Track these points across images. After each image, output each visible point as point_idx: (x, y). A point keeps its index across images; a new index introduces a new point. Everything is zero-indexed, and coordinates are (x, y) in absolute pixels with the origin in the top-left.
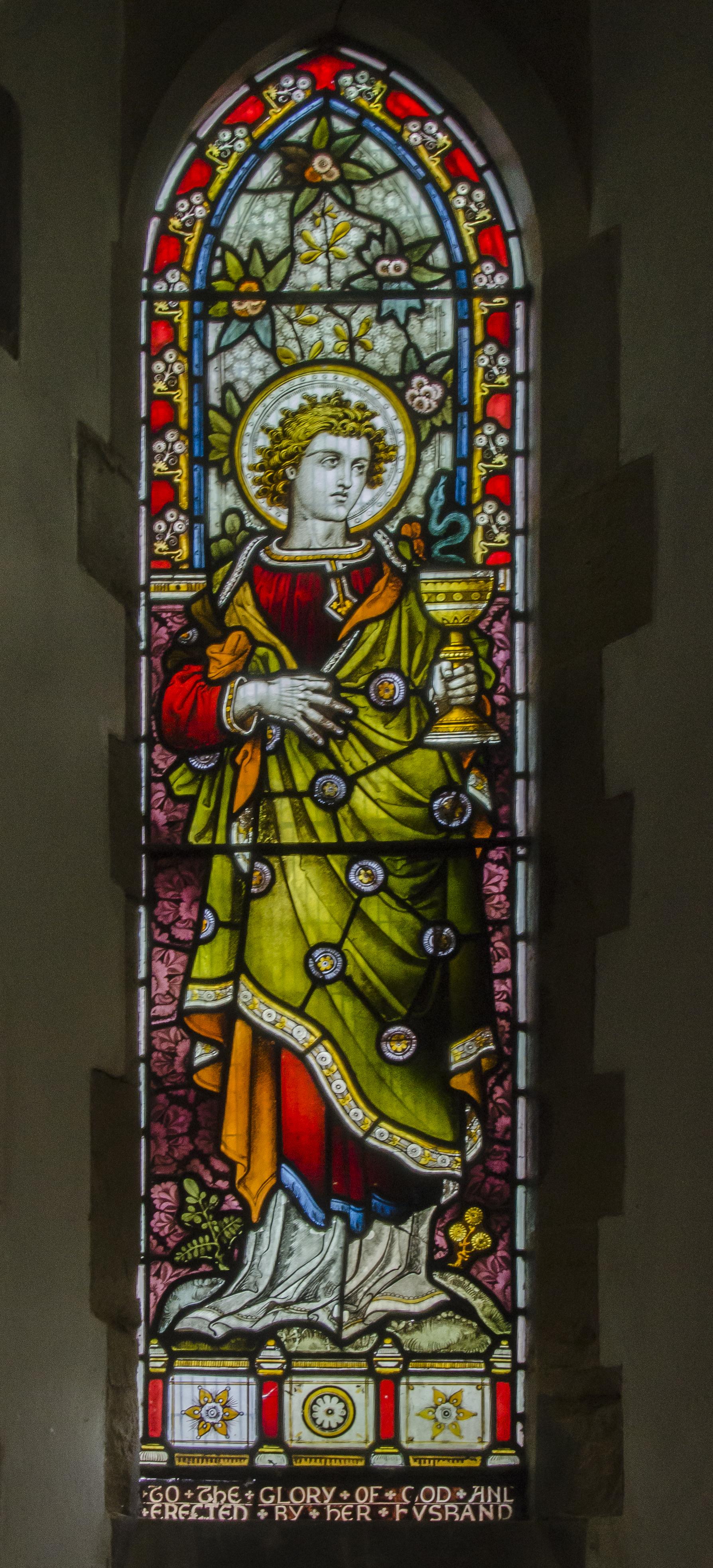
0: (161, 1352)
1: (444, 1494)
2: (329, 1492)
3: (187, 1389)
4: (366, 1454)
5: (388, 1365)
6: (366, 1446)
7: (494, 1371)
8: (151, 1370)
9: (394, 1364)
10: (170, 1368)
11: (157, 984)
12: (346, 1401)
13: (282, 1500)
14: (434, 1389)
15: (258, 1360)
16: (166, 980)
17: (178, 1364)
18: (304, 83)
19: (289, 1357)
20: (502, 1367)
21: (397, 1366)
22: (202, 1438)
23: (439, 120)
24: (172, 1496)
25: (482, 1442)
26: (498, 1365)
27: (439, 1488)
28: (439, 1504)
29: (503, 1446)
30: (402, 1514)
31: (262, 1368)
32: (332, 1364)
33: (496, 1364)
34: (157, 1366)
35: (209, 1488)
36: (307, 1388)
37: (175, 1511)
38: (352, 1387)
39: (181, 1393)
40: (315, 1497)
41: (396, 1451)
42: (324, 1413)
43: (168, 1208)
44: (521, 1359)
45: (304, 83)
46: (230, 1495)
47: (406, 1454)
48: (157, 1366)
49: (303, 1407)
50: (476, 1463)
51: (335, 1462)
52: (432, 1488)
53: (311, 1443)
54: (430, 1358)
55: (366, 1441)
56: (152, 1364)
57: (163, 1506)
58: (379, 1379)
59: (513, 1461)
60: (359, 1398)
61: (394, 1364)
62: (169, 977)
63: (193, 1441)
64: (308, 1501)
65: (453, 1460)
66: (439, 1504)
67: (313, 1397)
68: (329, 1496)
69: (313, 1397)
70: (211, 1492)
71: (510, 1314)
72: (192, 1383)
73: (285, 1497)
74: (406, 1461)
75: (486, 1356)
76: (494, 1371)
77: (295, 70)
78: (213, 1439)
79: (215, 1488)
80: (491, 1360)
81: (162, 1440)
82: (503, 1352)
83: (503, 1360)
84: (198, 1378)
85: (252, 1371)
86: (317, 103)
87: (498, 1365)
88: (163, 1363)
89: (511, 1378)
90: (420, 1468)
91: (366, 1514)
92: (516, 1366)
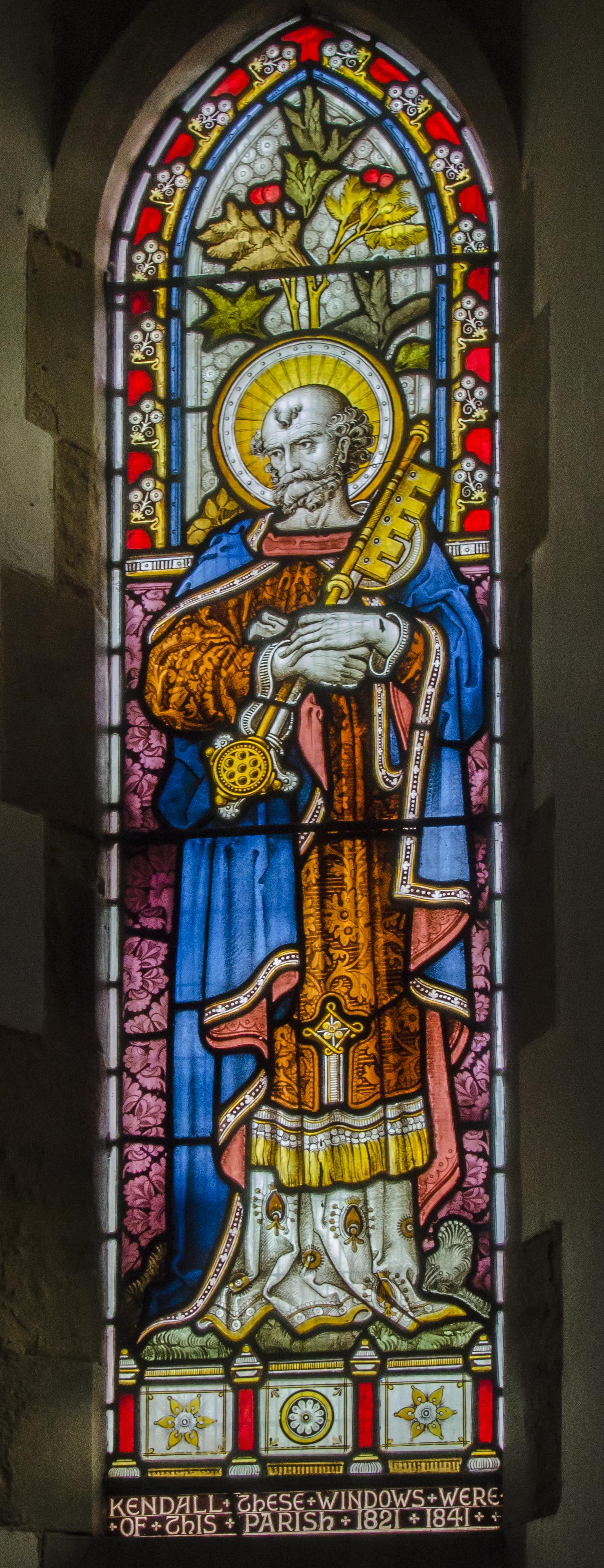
0: (132, 1363)
6: (222, 1456)
8: (121, 1382)
9: (370, 1367)
10: (382, 1370)
11: (129, 979)
12: (325, 1407)
15: (233, 1369)
16: (140, 974)
17: (149, 1374)
18: (290, 52)
19: (384, 1356)
20: (482, 1364)
23: (186, 118)
24: (371, 1502)
25: (223, 1451)
26: (240, 1374)
27: (162, 1499)
28: (212, 1514)
29: (366, 1451)
30: (140, 1529)
31: (238, 1377)
33: (476, 1361)
34: (127, 1378)
35: (247, 1497)
36: (284, 1393)
38: (327, 1389)
40: (481, 1499)
43: (472, 1193)
45: (290, 52)
46: (269, 1503)
47: (263, 1461)
48: (127, 1378)
49: (281, 1411)
51: (307, 1470)
55: (223, 1450)
56: (122, 1376)
60: (337, 1402)
61: (370, 1367)
62: (143, 971)
65: (175, 1471)
66: (212, 1514)
70: (251, 1500)
71: (495, 1308)
74: (264, 1469)
76: (474, 1369)
77: (278, 40)
79: (255, 1496)
81: (134, 1455)
82: (482, 1348)
83: (482, 1356)
85: (347, 1372)
86: (302, 76)
87: (477, 1362)
88: (133, 1375)
90: (276, 1477)
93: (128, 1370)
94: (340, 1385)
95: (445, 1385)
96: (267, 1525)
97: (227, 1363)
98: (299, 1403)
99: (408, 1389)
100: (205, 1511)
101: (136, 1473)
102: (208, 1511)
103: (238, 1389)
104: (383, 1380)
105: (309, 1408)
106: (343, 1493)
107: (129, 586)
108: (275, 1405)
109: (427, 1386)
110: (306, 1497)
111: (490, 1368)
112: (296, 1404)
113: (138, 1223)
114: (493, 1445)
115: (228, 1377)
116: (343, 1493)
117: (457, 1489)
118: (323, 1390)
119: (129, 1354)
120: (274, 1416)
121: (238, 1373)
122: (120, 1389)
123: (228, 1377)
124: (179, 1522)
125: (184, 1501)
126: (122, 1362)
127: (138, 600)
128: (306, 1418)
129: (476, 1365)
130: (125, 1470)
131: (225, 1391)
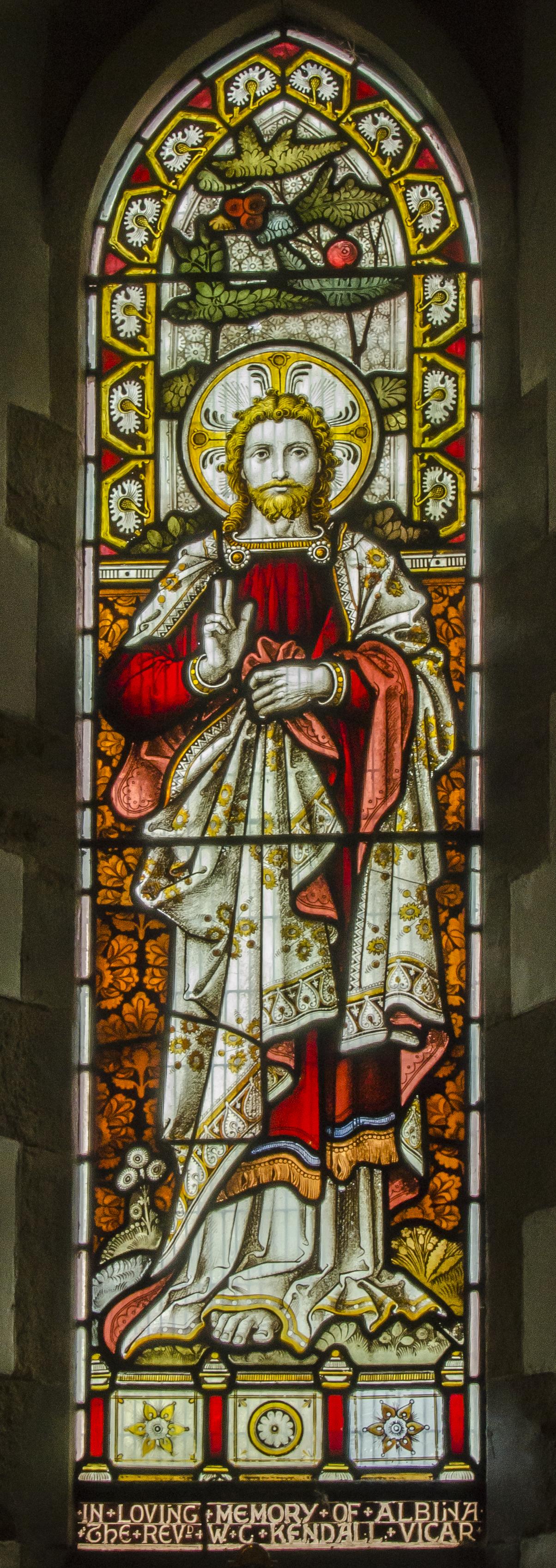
1: (292, 1510)
2: (309, 1510)
3: (368, 1403)
4: (315, 1472)
5: (214, 1381)
6: (192, 1465)
7: (324, 1384)
8: (93, 1387)
10: (232, 1385)
12: (295, 1418)
13: (124, 1518)
14: (145, 1404)
20: (454, 1379)
21: (105, 1383)
22: (144, 1458)
26: (329, 1378)
31: (207, 1383)
32: (171, 1377)
33: (447, 1376)
34: (100, 1383)
37: (155, 1532)
39: (361, 1406)
41: (347, 1468)
42: (280, 1428)
44: (474, 1372)
47: (116, 1472)
48: (100, 1383)
50: (426, 1477)
52: (140, 1507)
53: (301, 1460)
54: (366, 1371)
56: (93, 1381)
57: (171, 1527)
58: (328, 1394)
59: (470, 1476)
60: (307, 1413)
63: (374, 1460)
64: (287, 1518)
67: (257, 1414)
68: (310, 1514)
69: (257, 1414)
72: (374, 1397)
73: (126, 1516)
75: (195, 1371)
76: (204, 1386)
78: (397, 1456)
80: (443, 1372)
82: (455, 1364)
83: (454, 1371)
84: (143, 1393)
85: (317, 1385)
89: (463, 1391)
91: (468, 1534)
92: (468, 1380)
93: (98, 1375)
94: (310, 1397)
95: (177, 1401)
96: (447, 1533)
97: (315, 1369)
98: (278, 1413)
99: (140, 1406)
100: (411, 1519)
101: (108, 1477)
102: (414, 1519)
103: (328, 1394)
104: (319, 1395)
105: (279, 1419)
106: (162, 1507)
107: (101, 592)
108: (243, 1415)
109: (161, 1401)
110: (361, 1510)
111: (461, 1383)
112: (265, 1414)
113: (448, 1214)
114: (468, 1459)
115: (198, 1385)
116: (162, 1507)
117: (85, 1506)
118: (292, 1402)
119: (100, 1358)
120: (242, 1427)
121: (326, 1377)
122: (91, 1394)
123: (198, 1385)
124: (101, 1530)
125: (472, 1507)
126: (93, 1367)
127: (109, 605)
128: (275, 1429)
129: (207, 1383)
130: (97, 1474)
131: (116, 1398)
